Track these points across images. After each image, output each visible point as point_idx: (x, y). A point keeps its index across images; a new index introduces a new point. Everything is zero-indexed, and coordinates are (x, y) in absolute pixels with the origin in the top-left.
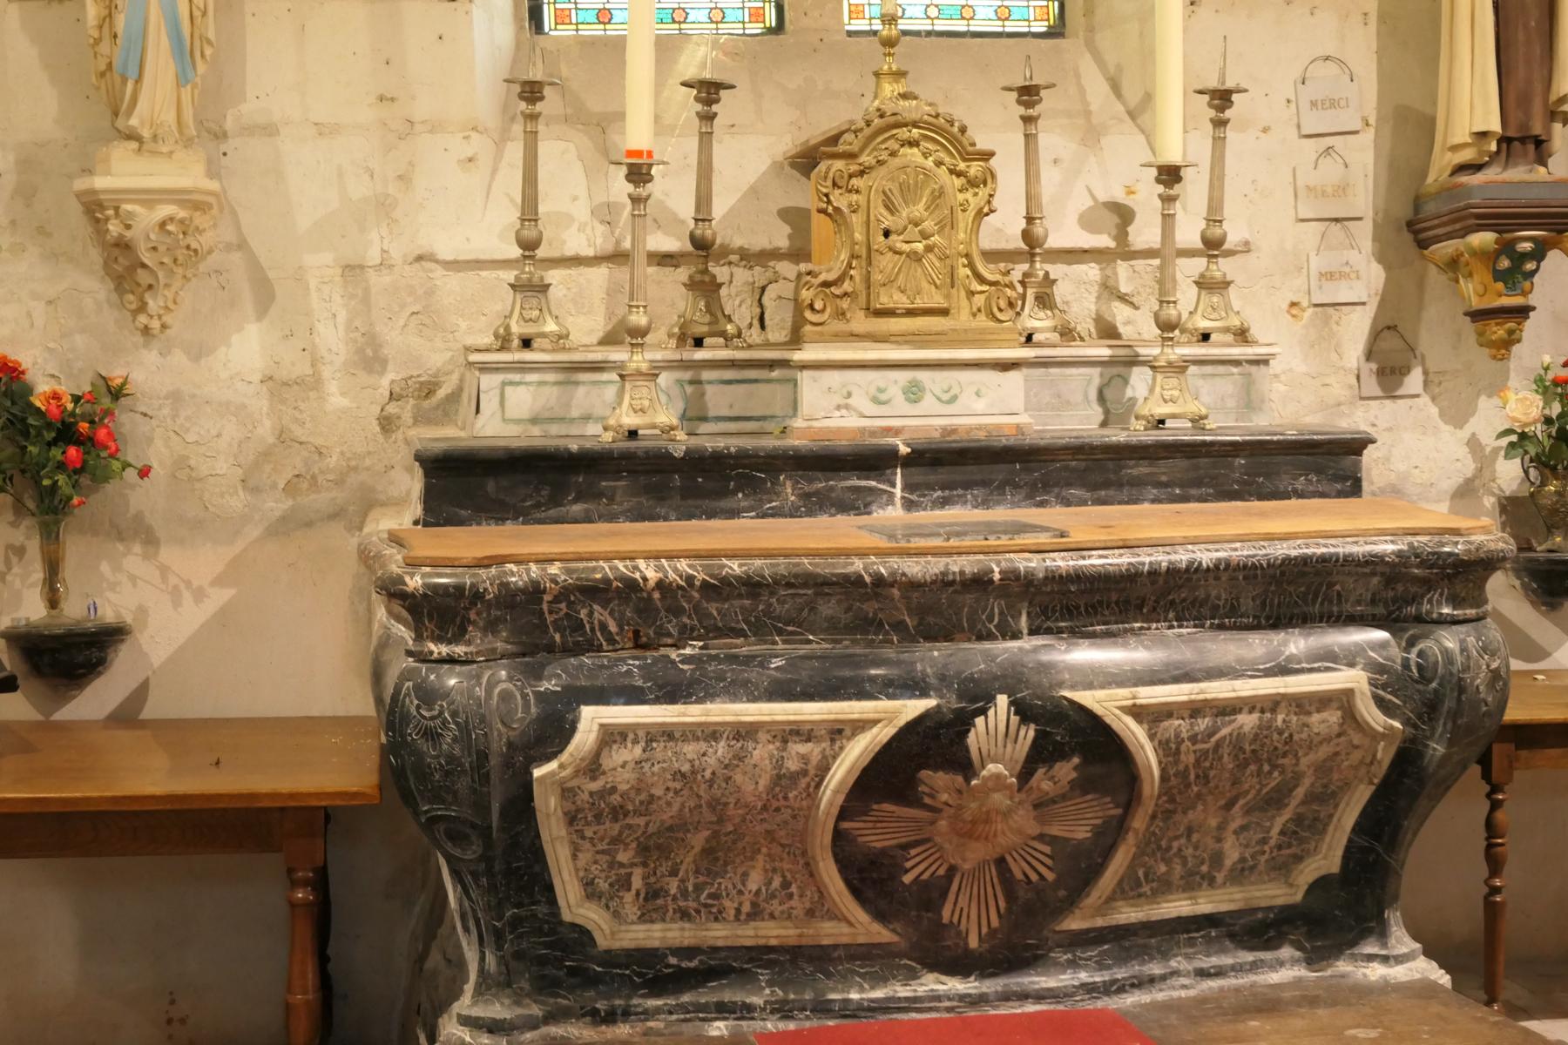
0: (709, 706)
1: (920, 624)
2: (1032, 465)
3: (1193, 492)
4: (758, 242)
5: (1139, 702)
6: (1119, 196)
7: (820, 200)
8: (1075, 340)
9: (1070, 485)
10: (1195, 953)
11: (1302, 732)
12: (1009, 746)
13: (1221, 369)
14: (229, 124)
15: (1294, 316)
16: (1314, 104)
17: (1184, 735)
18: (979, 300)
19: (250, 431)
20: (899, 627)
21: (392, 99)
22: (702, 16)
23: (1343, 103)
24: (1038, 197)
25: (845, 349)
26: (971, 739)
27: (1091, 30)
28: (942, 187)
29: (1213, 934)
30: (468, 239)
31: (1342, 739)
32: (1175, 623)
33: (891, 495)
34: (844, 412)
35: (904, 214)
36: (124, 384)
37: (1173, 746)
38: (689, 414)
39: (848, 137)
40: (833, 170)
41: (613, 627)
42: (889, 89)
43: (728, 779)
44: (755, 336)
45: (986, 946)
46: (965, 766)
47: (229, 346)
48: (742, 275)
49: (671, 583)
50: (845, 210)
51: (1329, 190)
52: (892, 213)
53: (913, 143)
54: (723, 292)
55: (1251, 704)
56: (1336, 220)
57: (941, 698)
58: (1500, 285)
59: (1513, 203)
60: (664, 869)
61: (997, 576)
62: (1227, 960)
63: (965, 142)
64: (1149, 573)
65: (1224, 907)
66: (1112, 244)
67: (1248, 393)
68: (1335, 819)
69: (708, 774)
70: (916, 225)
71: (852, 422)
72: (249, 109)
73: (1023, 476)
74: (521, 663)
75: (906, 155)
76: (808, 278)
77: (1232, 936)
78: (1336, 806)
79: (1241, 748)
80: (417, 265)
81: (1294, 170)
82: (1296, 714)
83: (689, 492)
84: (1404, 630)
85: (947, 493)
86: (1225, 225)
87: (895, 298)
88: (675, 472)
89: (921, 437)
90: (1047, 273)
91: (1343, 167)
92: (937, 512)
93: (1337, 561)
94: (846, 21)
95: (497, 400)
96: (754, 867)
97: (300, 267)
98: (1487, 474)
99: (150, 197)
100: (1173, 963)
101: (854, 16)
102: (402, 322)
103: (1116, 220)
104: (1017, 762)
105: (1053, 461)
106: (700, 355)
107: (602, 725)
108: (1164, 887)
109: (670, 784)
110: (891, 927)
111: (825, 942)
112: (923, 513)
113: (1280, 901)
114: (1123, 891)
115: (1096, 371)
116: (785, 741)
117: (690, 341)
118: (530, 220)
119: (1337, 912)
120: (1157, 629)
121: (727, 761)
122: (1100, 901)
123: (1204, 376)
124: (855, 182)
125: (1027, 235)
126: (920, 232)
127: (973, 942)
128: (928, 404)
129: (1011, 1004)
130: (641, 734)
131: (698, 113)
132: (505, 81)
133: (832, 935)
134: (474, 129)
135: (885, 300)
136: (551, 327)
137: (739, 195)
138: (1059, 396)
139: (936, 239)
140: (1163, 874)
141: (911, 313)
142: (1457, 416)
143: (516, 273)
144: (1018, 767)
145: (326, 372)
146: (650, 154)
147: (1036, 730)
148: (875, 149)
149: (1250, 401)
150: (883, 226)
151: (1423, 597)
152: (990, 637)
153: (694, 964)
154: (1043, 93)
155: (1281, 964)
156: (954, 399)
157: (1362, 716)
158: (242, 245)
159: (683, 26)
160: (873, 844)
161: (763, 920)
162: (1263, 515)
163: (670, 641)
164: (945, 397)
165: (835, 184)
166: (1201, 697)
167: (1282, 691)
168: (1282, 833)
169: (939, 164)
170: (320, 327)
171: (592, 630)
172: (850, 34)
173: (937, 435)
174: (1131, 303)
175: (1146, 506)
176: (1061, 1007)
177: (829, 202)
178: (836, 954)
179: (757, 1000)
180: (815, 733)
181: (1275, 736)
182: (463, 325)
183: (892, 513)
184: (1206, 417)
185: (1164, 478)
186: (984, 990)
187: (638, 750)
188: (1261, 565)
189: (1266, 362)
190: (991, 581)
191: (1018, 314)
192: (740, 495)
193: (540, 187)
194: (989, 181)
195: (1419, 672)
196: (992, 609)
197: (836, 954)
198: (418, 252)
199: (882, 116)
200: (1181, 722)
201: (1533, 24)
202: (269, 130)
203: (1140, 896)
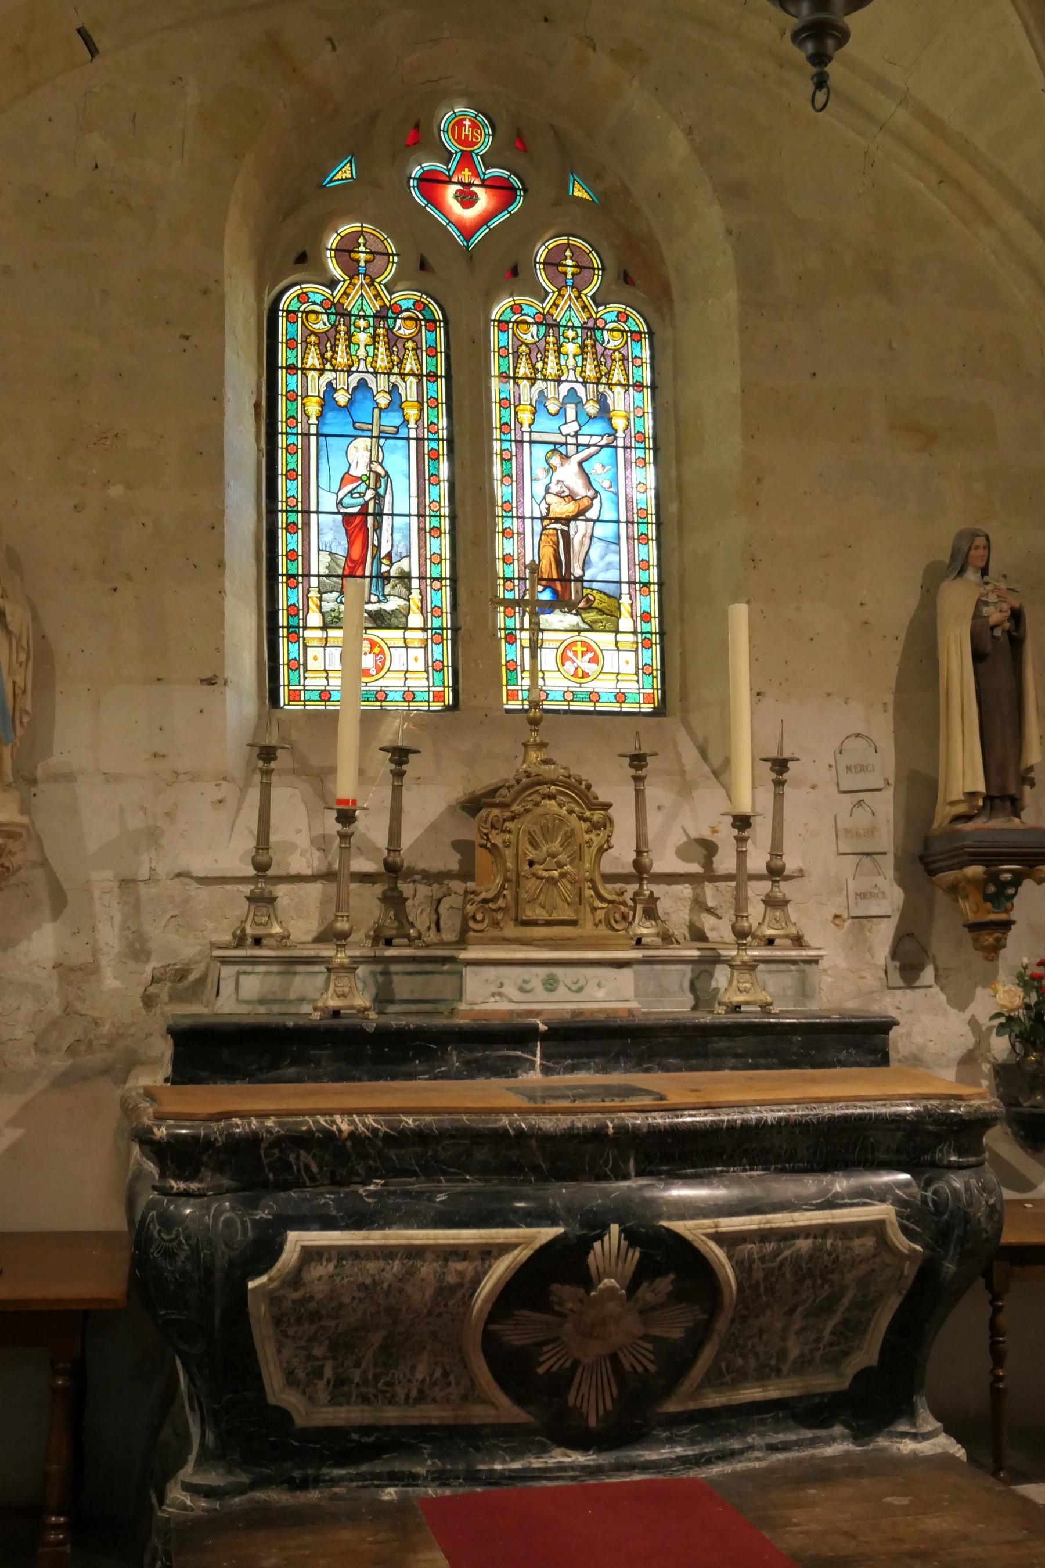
3: (762, 1061)
5: (720, 1230)
9: (668, 1055)
13: (783, 967)
14: (40, 773)
15: (837, 925)
20: (536, 1169)
21: (163, 756)
22: (398, 696)
23: (870, 768)
27: (685, 711)
29: (780, 1415)
32: (748, 1167)
33: (533, 1063)
34: (497, 998)
40: (491, 816)
41: (315, 1168)
47: (30, 939)
49: (360, 1134)
51: (861, 832)
55: (806, 1232)
56: (867, 854)
58: (989, 905)
61: (611, 1131)
64: (727, 1128)
65: (789, 1393)
69: (385, 1286)
71: (504, 1006)
80: (177, 880)
86: (785, 859)
87: (537, 911)
91: (871, 815)
92: (568, 1076)
95: (233, 985)
97: (88, 881)
100: (749, 1440)
102: (163, 924)
107: (303, 1247)
108: (741, 1378)
111: (476, 1421)
113: (832, 1389)
116: (446, 1260)
120: (734, 1171)
123: (769, 972)
124: (508, 825)
128: (562, 992)
135: (529, 914)
141: (549, 923)
144: (627, 1282)
145: (103, 961)
147: (641, 1253)
148: (523, 801)
149: (804, 991)
151: (936, 1147)
152: (606, 1178)
155: (834, 1440)
156: (580, 990)
159: (384, 704)
162: (814, 1081)
164: (575, 987)
165: (493, 827)
166: (768, 1226)
167: (830, 1221)
169: (570, 812)
171: (299, 1170)
172: (508, 711)
173: (568, 1016)
175: (727, 1072)
177: (488, 839)
179: (420, 1470)
181: (826, 1257)
183: (534, 1077)
184: (771, 1004)
185: (740, 1051)
186: (601, 1461)
187: (331, 1267)
190: (607, 1134)
192: (417, 1062)
196: (608, 1155)
200: (753, 1245)
202: (68, 777)
203: (722, 1384)
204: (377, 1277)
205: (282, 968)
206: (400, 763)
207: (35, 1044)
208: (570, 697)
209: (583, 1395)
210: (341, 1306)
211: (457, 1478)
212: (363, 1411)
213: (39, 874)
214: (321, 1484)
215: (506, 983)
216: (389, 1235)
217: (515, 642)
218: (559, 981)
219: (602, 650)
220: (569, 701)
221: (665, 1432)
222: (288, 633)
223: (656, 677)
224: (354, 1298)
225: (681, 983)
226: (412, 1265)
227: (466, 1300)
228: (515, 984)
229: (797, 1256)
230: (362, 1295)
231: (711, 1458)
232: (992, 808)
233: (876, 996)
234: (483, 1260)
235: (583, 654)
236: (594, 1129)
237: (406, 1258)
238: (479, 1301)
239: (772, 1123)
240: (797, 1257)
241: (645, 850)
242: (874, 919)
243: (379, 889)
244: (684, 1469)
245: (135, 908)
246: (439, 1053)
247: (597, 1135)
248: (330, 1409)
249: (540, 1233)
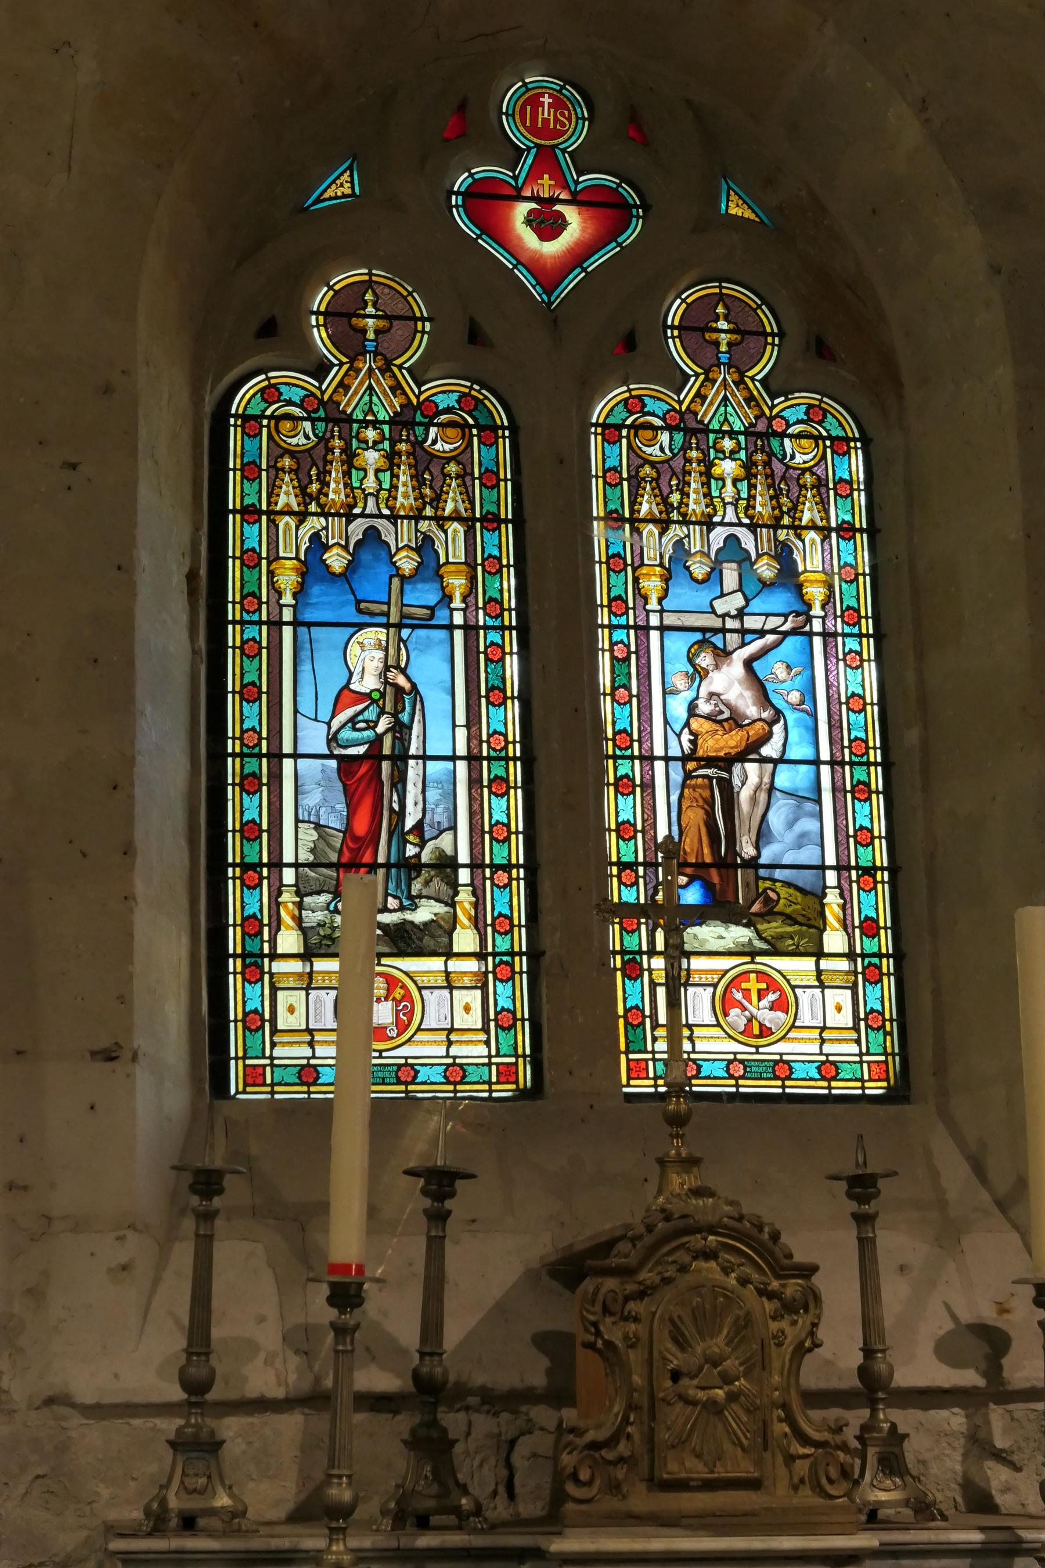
4: (505, 1380)
6: (988, 1314)
7: (587, 1330)
8: (934, 1519)
18: (802, 1468)
21: (25, 1188)
24: (880, 1320)
30: (116, 1376)
35: (699, 1350)
39: (623, 1247)
40: (603, 1290)
42: (677, 1181)
44: (500, 1508)
48: (484, 1424)
50: (620, 1344)
52: (683, 1349)
53: (709, 1255)
54: (458, 1448)
63: (779, 1254)
66: (981, 1382)
70: (715, 1364)
75: (699, 1271)
76: (571, 1437)
87: (688, 1464)
90: (894, 1426)
94: (624, 1081)
101: (633, 1075)
102: (22, 1489)
103: (986, 1349)
106: (425, 1541)
117: (411, 1521)
124: (632, 1306)
125: (864, 1372)
126: (719, 1373)
131: (426, 1211)
132: (174, 1168)
134: (132, 1227)
135: (673, 1468)
136: (223, 1500)
137: (479, 1316)
139: (741, 1383)
141: (710, 1485)
143: (180, 1422)
146: (360, 1269)
148: (658, 1263)
150: (671, 1366)
154: (881, 1183)
159: (411, 1088)
165: (606, 1310)
169: (744, 1282)
172: (630, 1097)
177: (598, 1334)
182: (105, 1492)
191: (857, 1483)
193: (215, 1303)
194: (812, 1305)
198: (51, 1393)
199: (668, 1219)
222: (244, 966)
223: (891, 1034)
241: (880, 1347)
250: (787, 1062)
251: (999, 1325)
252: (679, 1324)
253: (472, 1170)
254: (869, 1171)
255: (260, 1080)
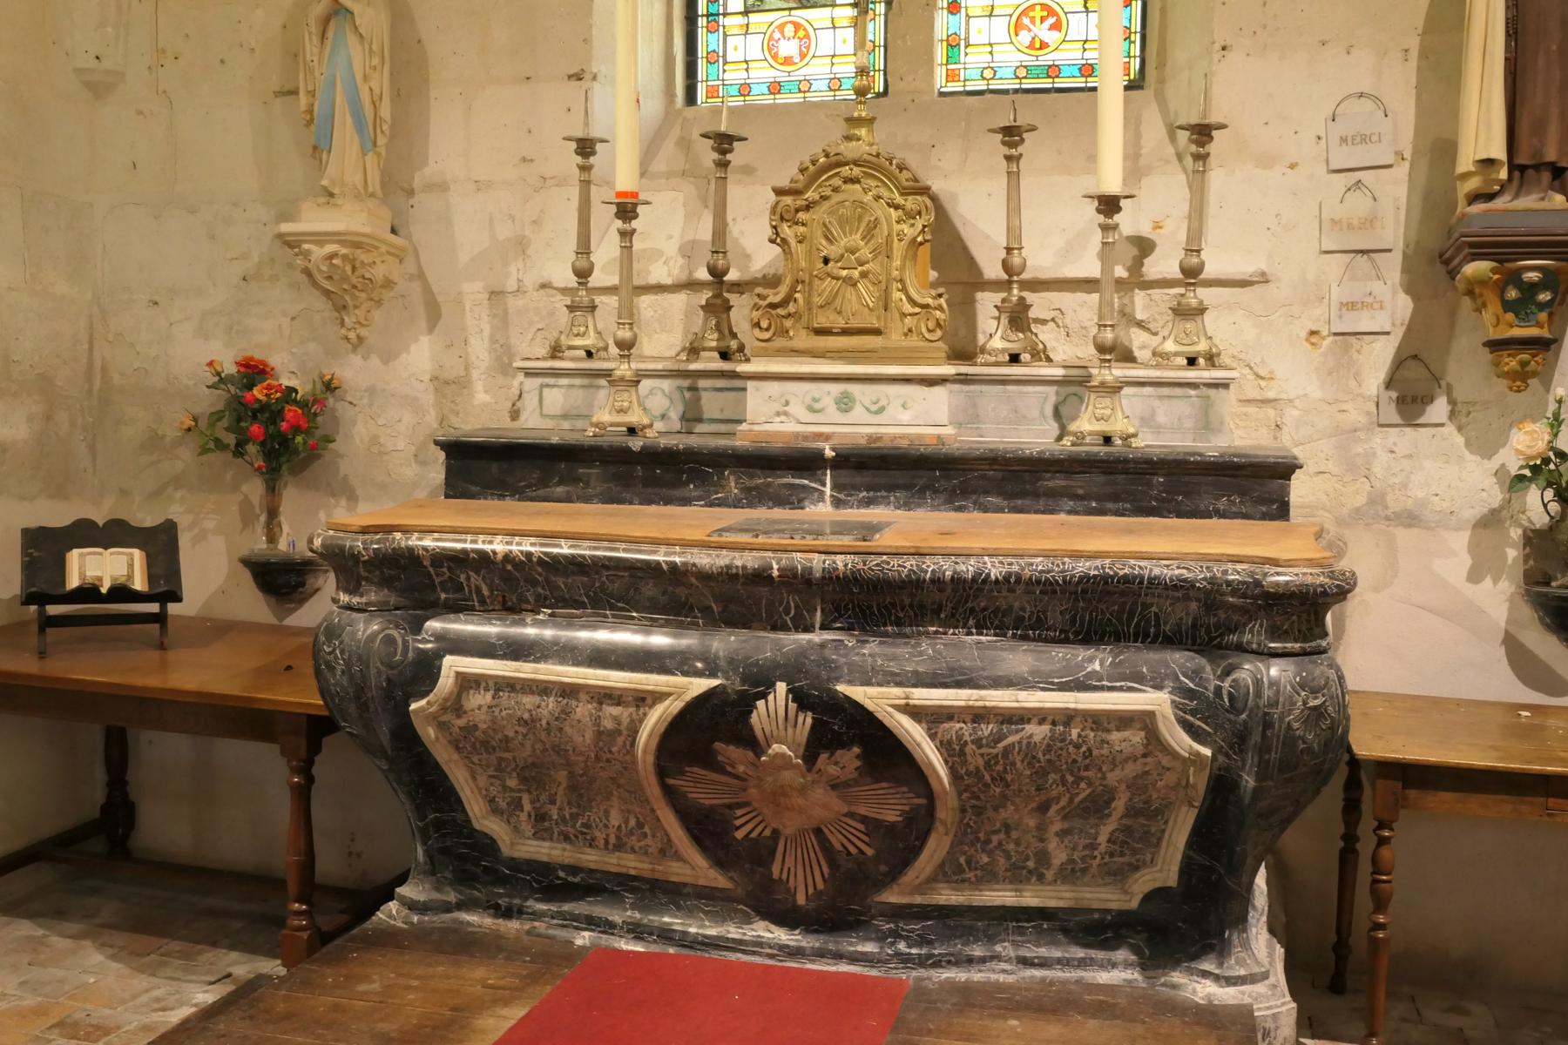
0: (542, 666)
1: (724, 611)
2: (952, 473)
3: (1110, 505)
5: (911, 702)
8: (1041, 360)
9: (987, 493)
10: (1024, 942)
11: (1102, 748)
12: (790, 730)
13: (1178, 391)
14: (416, 184)
15: (1313, 344)
16: (1344, 140)
17: (967, 738)
19: (421, 418)
20: (706, 610)
21: (532, 160)
22: (823, 85)
23: (1375, 138)
25: (785, 363)
26: (754, 719)
27: (1161, 81)
28: (876, 219)
29: (1045, 926)
31: (1149, 759)
32: (974, 631)
33: (822, 493)
34: (783, 418)
35: (842, 243)
36: (331, 380)
37: (957, 748)
38: (687, 416)
40: (781, 205)
41: (486, 592)
43: (561, 730)
45: (812, 905)
46: (752, 743)
47: (409, 352)
49: (514, 558)
51: (1355, 222)
55: (1041, 716)
56: (1363, 252)
57: (727, 679)
58: (1510, 316)
59: (1554, 232)
60: (544, 797)
61: (775, 573)
62: (1057, 953)
64: (932, 581)
65: (1052, 903)
67: (1207, 414)
68: (1166, 836)
69: (544, 722)
71: (790, 427)
72: (429, 172)
73: (942, 483)
74: (411, 615)
77: (1066, 931)
78: (1166, 823)
79: (1034, 757)
80: (542, 292)
81: (1321, 203)
82: (1092, 729)
83: (650, 481)
84: (1223, 657)
85: (871, 494)
86: (1204, 255)
87: (831, 318)
88: (638, 464)
89: (848, 443)
91: (1372, 200)
92: (863, 511)
93: (1141, 582)
95: (536, 399)
96: (612, 806)
98: (1516, 505)
99: (321, 238)
100: (998, 948)
103: (1135, 252)
104: (799, 745)
105: (971, 470)
107: (458, 674)
108: (988, 877)
109: (517, 728)
110: (730, 875)
111: (674, 879)
112: (850, 510)
113: (1114, 906)
114: (945, 874)
115: (1052, 390)
116: (601, 703)
118: (582, 253)
119: (1180, 924)
120: (954, 634)
121: (557, 715)
122: (917, 882)
123: (1161, 397)
124: (802, 216)
127: (801, 900)
128: (858, 413)
129: (825, 960)
130: (491, 684)
133: (678, 874)
135: (822, 320)
138: (1016, 411)
140: (986, 864)
141: (846, 332)
142: (1485, 446)
144: (802, 749)
145: (475, 374)
147: (813, 718)
148: (820, 186)
149: (1207, 424)
150: (823, 254)
151: (1245, 625)
152: (784, 628)
153: (577, 880)
155: (1114, 965)
156: (881, 410)
157: (1166, 740)
158: (421, 276)
159: (807, 95)
160: (702, 801)
161: (626, 852)
162: (1129, 531)
163: (529, 607)
164: (874, 408)
165: (782, 219)
166: (980, 704)
167: (1072, 706)
168: (1109, 841)
169: (878, 198)
170: (472, 340)
171: (470, 591)
172: (942, 94)
173: (863, 442)
174: (1149, 329)
175: (1063, 516)
176: (874, 973)
177: (777, 234)
178: (685, 891)
179: (617, 918)
180: (624, 699)
181: (1071, 749)
183: (822, 510)
184: (1135, 435)
185: (1080, 492)
186: (804, 944)
187: (489, 696)
188: (1057, 581)
189: (1226, 386)
190: (770, 577)
192: (692, 486)
194: (924, 212)
195: (1230, 701)
196: (788, 602)
197: (685, 891)
200: (963, 725)
201: (1554, 47)
202: (442, 187)
203: (963, 881)
204: (534, 713)
205: (585, 381)
206: (724, 152)
207: (415, 456)
208: (989, 74)
209: (789, 869)
210: (507, 739)
211: (651, 934)
212: (564, 850)
213: (416, 285)
214: (525, 916)
215: (792, 400)
216: (539, 669)
217: (959, 11)
218: (855, 400)
219: (1066, 13)
220: (988, 80)
221: (888, 923)
222: (708, 22)
223: (1134, 42)
224: (516, 732)
225: (1042, 408)
226: (567, 704)
227: (628, 747)
228: (803, 402)
229: (1029, 743)
230: (524, 730)
231: (940, 961)
232: (1521, 184)
233: (1361, 435)
234: (638, 706)
235: (1043, 19)
236: (755, 569)
237: (561, 696)
238: (640, 752)
239: (997, 579)
240: (1029, 748)
241: (1016, 246)
242: (1365, 337)
243: (704, 296)
244: (903, 968)
245: (502, 320)
246: (716, 478)
247: (760, 577)
248: (535, 843)
249: (691, 683)
250: (1057, 66)
251: (1151, 237)
252: (829, 226)
253: (745, 136)
254: (1017, 124)
255: (715, 95)
